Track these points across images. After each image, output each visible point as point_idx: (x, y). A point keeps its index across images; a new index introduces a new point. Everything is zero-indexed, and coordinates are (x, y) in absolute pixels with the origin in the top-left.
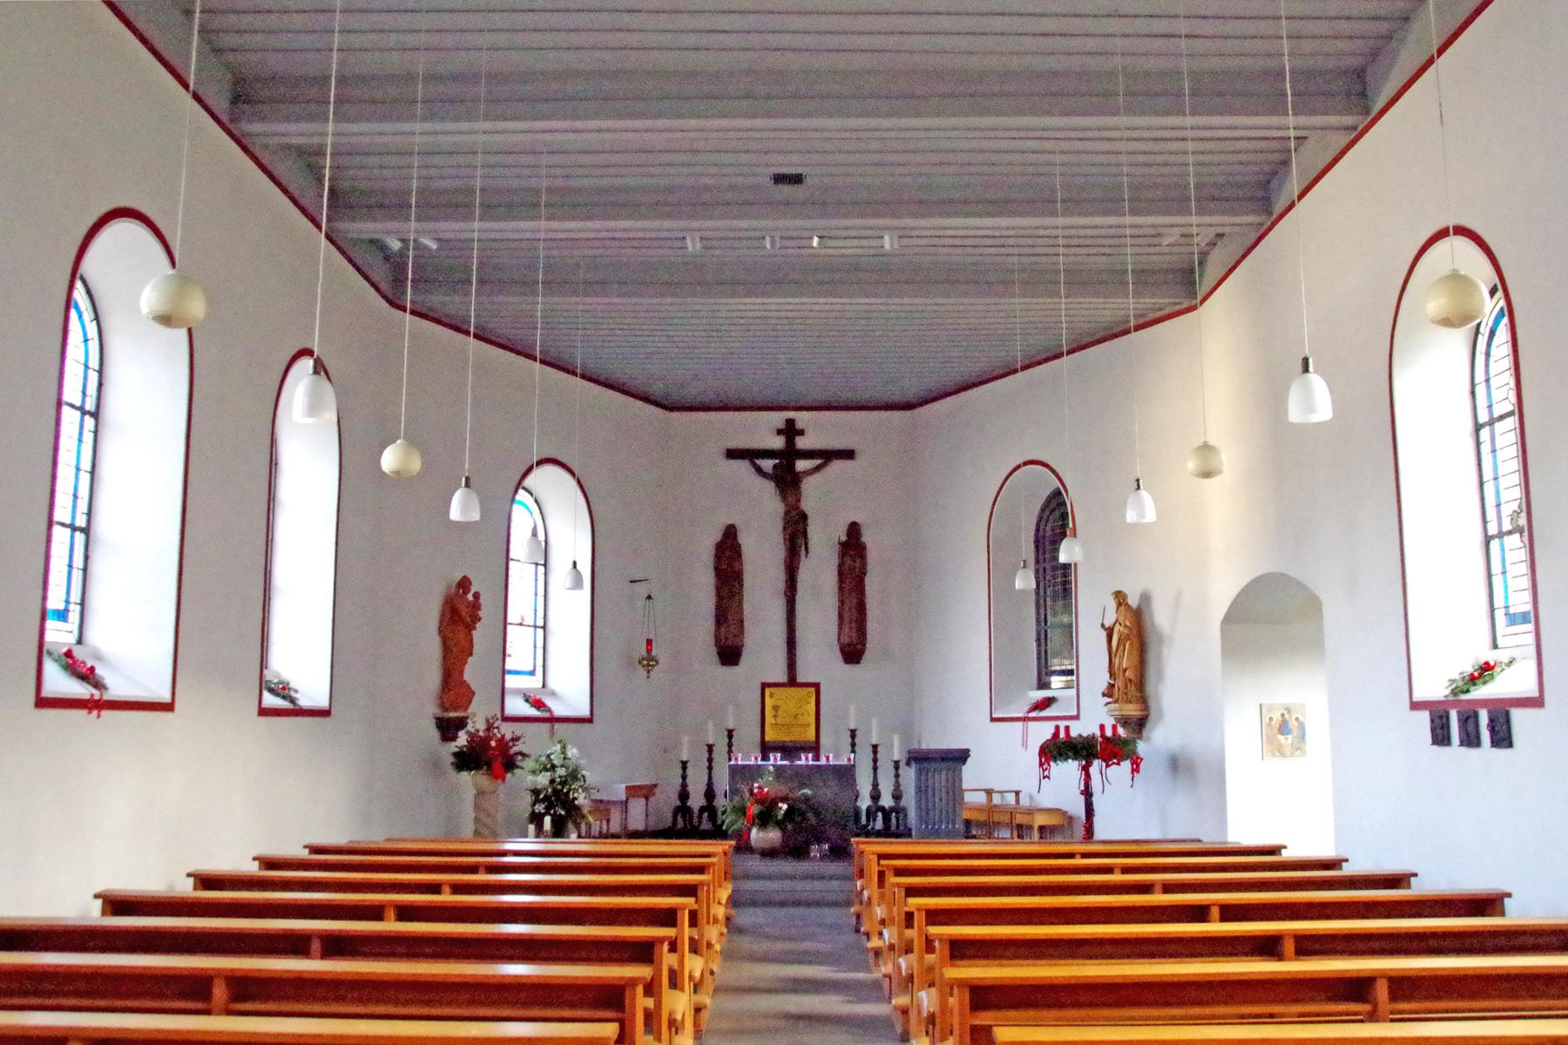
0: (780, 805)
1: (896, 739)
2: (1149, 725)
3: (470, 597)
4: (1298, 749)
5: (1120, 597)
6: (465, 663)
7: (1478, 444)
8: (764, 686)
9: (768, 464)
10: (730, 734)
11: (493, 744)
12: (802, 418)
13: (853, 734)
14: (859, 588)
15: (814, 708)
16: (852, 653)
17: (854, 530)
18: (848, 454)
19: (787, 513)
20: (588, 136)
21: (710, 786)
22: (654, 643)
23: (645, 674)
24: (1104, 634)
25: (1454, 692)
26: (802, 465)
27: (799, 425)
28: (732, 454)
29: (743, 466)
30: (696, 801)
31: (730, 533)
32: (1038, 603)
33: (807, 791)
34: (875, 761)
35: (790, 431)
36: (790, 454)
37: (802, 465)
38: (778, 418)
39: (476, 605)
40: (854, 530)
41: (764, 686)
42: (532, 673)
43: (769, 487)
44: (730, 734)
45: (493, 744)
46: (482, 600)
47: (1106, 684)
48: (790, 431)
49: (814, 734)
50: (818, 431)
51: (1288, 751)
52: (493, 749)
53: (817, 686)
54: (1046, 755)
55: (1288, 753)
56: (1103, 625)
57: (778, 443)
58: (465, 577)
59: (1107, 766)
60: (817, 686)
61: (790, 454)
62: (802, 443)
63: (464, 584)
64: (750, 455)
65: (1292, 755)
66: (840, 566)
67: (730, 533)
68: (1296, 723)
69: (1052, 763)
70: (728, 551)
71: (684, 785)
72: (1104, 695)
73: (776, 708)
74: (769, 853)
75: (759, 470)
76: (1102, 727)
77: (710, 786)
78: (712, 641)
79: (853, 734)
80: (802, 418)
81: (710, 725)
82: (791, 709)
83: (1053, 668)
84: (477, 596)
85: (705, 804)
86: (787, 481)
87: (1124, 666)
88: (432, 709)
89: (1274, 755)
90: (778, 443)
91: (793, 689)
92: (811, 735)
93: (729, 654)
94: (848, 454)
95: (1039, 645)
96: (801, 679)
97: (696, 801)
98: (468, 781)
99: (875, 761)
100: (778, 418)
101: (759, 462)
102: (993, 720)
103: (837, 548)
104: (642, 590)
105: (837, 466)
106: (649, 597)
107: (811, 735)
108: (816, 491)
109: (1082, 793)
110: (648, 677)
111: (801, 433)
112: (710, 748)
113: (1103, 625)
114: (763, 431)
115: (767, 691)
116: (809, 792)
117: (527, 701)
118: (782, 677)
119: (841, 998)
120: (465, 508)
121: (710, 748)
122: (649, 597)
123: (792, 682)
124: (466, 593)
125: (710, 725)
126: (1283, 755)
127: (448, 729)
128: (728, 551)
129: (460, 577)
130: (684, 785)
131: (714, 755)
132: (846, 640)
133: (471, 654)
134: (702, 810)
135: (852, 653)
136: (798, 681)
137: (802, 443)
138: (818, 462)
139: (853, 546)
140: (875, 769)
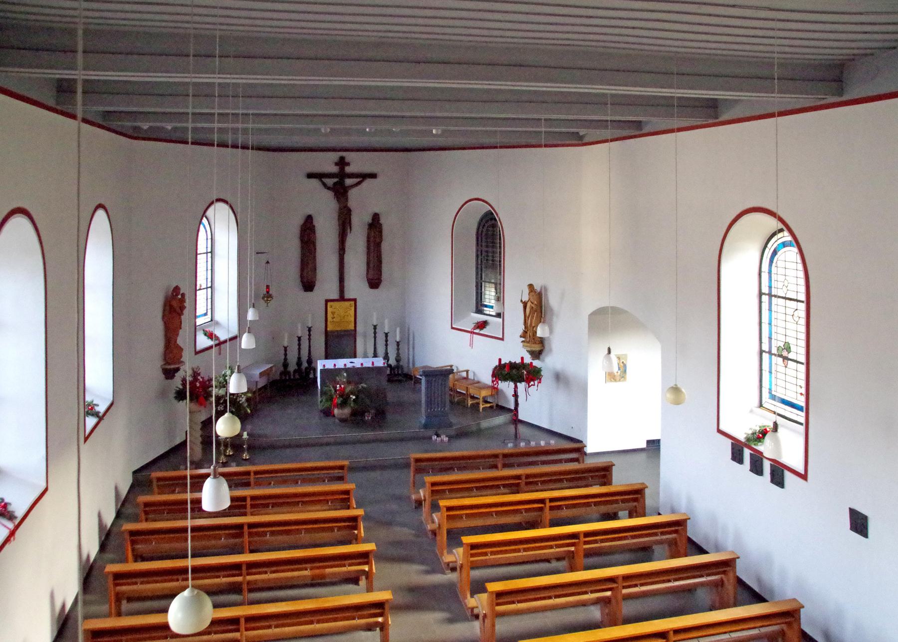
0: (351, 396)
1: (398, 330)
2: (544, 354)
3: (180, 297)
4: (623, 377)
5: (531, 286)
6: (177, 335)
7: (760, 302)
8: (327, 301)
9: (330, 182)
10: (310, 330)
11: (198, 384)
12: (349, 156)
13: (375, 327)
14: (378, 245)
15: (353, 312)
16: (374, 282)
17: (376, 217)
18: (373, 176)
19: (340, 209)
20: (406, 350)
21: (299, 358)
22: (270, 287)
23: (266, 304)
24: (522, 305)
25: (748, 439)
26: (349, 182)
27: (347, 160)
28: (310, 176)
29: (315, 182)
30: (292, 367)
31: (309, 219)
32: (477, 268)
33: (364, 385)
34: (386, 341)
35: (342, 163)
36: (342, 175)
37: (349, 182)
38: (335, 156)
39: (183, 300)
40: (376, 217)
41: (327, 301)
42: (206, 314)
43: (330, 194)
44: (310, 330)
45: (198, 384)
46: (187, 297)
47: (522, 331)
48: (342, 163)
49: (353, 325)
50: (358, 163)
51: (618, 378)
52: (198, 388)
53: (355, 300)
54: (495, 377)
55: (618, 380)
56: (521, 301)
57: (335, 169)
58: (177, 286)
59: (529, 387)
60: (355, 300)
61: (342, 175)
62: (348, 169)
63: (177, 289)
64: (319, 176)
65: (620, 380)
66: (368, 238)
67: (309, 219)
68: (622, 364)
69: (500, 382)
70: (308, 229)
71: (286, 359)
72: (521, 337)
73: (333, 313)
74: (343, 421)
75: (325, 185)
76: (522, 358)
77: (299, 358)
78: (299, 280)
79: (375, 327)
80: (349, 156)
81: (299, 326)
82: (341, 312)
83: (485, 303)
84: (183, 295)
85: (297, 368)
86: (340, 192)
87: (533, 325)
88: (158, 363)
89: (611, 381)
90: (335, 169)
91: (343, 302)
92: (352, 327)
93: (308, 285)
94: (373, 176)
95: (477, 289)
96: (347, 296)
97: (292, 367)
98: (185, 406)
99: (386, 341)
100: (335, 156)
101: (324, 180)
102: (452, 328)
103: (367, 227)
104: (264, 258)
105: (368, 182)
106: (268, 262)
107: (352, 327)
108: (354, 196)
109: (513, 396)
110: (267, 306)
111: (348, 164)
112: (299, 339)
113: (521, 301)
114: (327, 163)
115: (329, 304)
116: (365, 386)
117: (205, 335)
118: (336, 296)
119: (439, 615)
120: (239, 385)
121: (299, 339)
122: (268, 262)
123: (342, 298)
124: (177, 295)
125: (299, 326)
126: (615, 381)
127: (169, 374)
128: (308, 229)
129: (174, 286)
130: (286, 359)
131: (301, 342)
132: (371, 277)
133: (181, 328)
134: (295, 371)
135: (374, 282)
136: (345, 298)
137: (348, 169)
138: (358, 180)
139: (375, 225)
140: (386, 345)
